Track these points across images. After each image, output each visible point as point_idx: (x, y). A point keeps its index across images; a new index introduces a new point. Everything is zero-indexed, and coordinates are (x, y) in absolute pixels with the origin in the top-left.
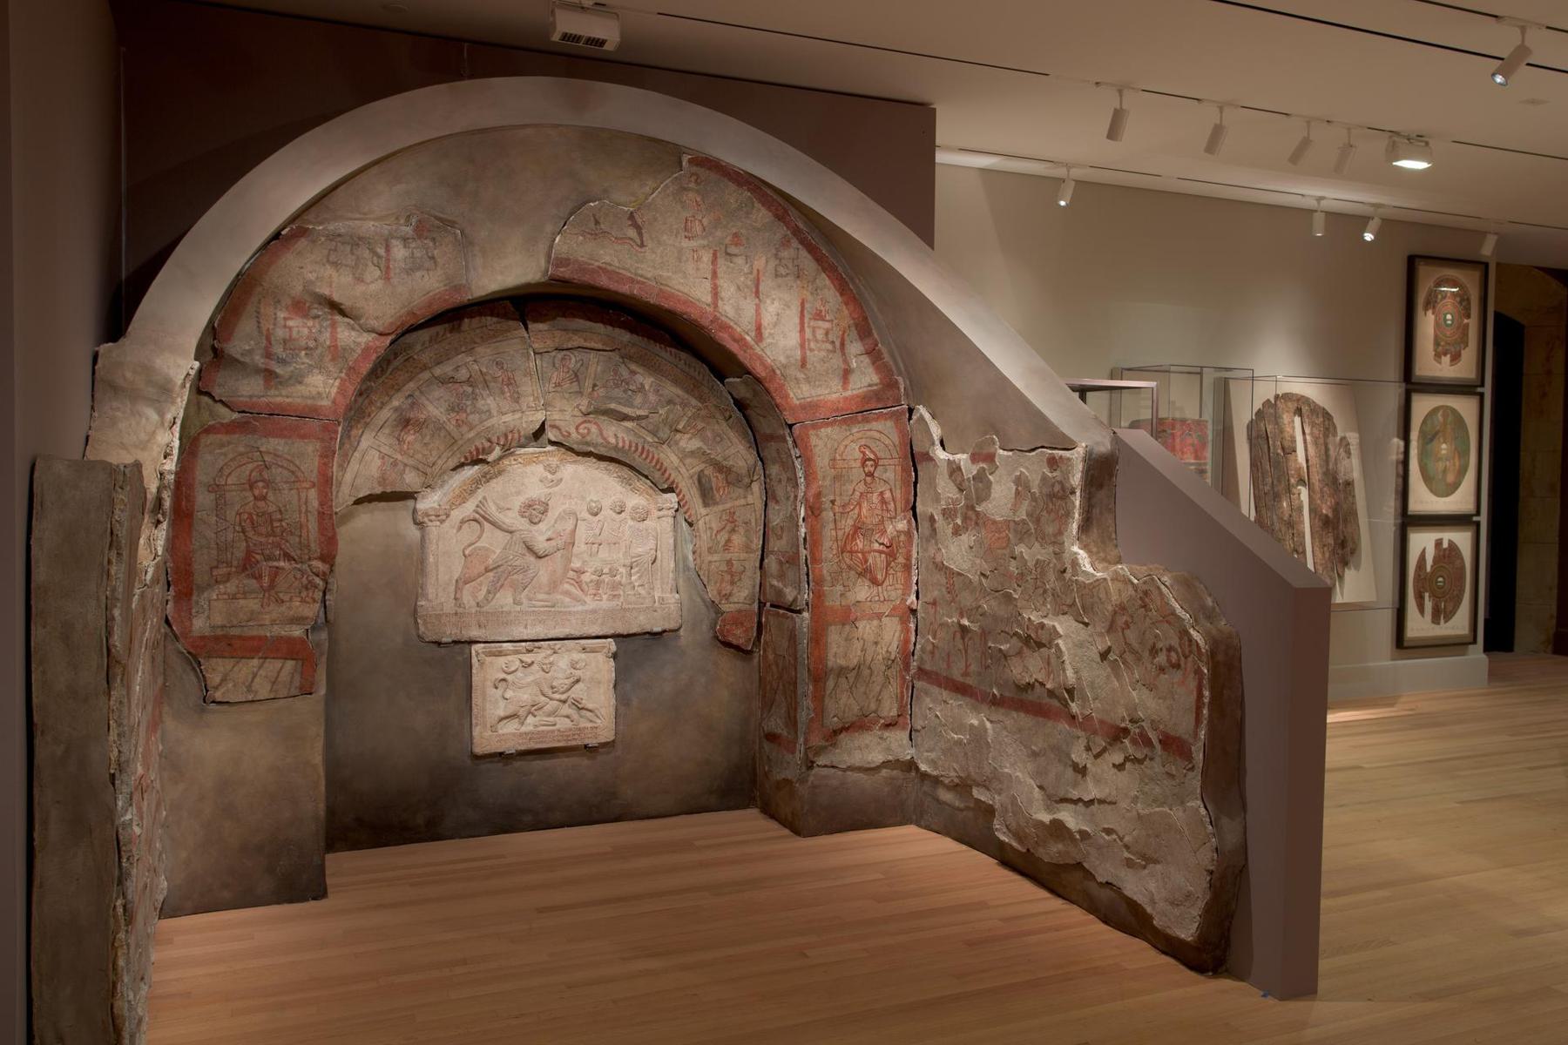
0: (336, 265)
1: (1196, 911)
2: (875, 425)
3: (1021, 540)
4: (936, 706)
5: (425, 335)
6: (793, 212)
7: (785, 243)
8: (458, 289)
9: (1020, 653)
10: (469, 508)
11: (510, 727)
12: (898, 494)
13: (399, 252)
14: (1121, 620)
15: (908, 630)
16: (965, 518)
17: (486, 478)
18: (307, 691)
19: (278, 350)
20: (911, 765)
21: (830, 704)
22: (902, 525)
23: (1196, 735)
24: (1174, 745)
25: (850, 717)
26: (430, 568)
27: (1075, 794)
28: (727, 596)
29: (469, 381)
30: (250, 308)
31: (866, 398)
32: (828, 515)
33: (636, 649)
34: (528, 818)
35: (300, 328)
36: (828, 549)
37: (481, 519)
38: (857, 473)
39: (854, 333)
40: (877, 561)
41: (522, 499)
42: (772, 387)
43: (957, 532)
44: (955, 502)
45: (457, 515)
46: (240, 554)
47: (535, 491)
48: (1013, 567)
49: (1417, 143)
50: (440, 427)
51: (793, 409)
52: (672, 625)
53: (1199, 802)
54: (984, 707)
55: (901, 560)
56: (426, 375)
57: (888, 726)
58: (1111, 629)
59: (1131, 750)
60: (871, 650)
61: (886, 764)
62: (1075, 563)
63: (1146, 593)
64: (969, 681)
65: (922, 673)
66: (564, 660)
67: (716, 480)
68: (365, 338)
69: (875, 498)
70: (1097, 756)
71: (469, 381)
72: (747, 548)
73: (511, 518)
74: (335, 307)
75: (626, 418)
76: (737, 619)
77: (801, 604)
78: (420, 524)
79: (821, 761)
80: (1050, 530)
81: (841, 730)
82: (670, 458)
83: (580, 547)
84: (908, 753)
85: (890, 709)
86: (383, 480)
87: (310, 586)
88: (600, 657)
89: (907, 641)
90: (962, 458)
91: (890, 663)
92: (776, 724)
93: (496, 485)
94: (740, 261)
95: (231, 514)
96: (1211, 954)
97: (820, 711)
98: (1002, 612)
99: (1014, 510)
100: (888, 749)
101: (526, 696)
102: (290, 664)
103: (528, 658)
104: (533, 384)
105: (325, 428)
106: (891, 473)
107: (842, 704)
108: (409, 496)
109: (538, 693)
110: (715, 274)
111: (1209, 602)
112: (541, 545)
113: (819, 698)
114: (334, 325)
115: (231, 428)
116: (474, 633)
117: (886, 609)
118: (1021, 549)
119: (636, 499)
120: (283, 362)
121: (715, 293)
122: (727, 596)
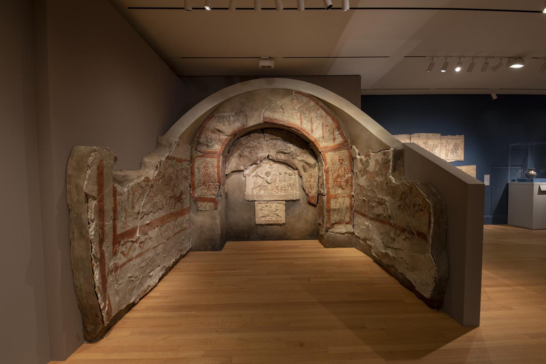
0: (219, 122)
1: (431, 288)
2: (342, 151)
3: (377, 176)
4: (359, 219)
5: (244, 138)
6: (320, 102)
7: (318, 109)
8: (244, 125)
9: (377, 206)
10: (254, 173)
11: (263, 219)
12: (349, 168)
13: (232, 118)
14: (404, 196)
15: (352, 201)
16: (364, 172)
17: (258, 167)
18: (216, 209)
19: (209, 140)
20: (353, 233)
21: (332, 218)
22: (350, 175)
23: (429, 233)
24: (422, 236)
25: (337, 221)
26: (247, 186)
27: (392, 246)
28: (310, 192)
29: (253, 147)
30: (204, 132)
31: (339, 145)
32: (330, 173)
33: (290, 203)
34: (268, 238)
35: (213, 136)
36: (331, 181)
37: (257, 176)
38: (338, 163)
39: (336, 129)
40: (343, 184)
41: (265, 171)
42: (315, 143)
43: (362, 176)
44: (361, 168)
45: (252, 175)
46: (203, 181)
47: (268, 170)
48: (375, 183)
49: (518, 59)
50: (247, 157)
51: (321, 148)
52: (298, 198)
53: (430, 254)
54: (369, 220)
55: (350, 184)
56: (244, 146)
57: (347, 223)
58: (401, 199)
59: (407, 235)
60: (342, 205)
61: (346, 233)
62: (391, 181)
63: (411, 188)
64: (366, 213)
65: (356, 211)
66: (274, 206)
67: (307, 167)
68: (226, 137)
69: (343, 169)
70: (398, 236)
71: (253, 147)
72: (315, 182)
73: (263, 176)
74: (219, 131)
75: (286, 153)
76: (313, 197)
77: (324, 194)
78: (245, 177)
79: (330, 231)
80: (384, 172)
81: (335, 223)
82: (296, 162)
83: (278, 181)
84: (352, 230)
85: (347, 219)
86: (236, 168)
87: (216, 188)
88: (282, 205)
89: (351, 203)
90: (363, 157)
91: (347, 208)
92: (320, 221)
93: (260, 168)
94: (307, 115)
95: (201, 174)
96: (436, 303)
97: (329, 219)
98: (372, 195)
99: (375, 169)
100: (347, 229)
101: (266, 213)
102: (213, 203)
103: (267, 205)
104: (268, 147)
105: (218, 156)
106: (347, 163)
107: (335, 217)
108: (242, 171)
109: (269, 213)
110: (301, 118)
111: (434, 190)
112: (269, 181)
113: (329, 216)
114: (219, 135)
115: (201, 156)
116: (256, 199)
117: (346, 195)
118: (377, 179)
119: (290, 171)
120: (210, 143)
121: (301, 123)
122: (310, 192)
